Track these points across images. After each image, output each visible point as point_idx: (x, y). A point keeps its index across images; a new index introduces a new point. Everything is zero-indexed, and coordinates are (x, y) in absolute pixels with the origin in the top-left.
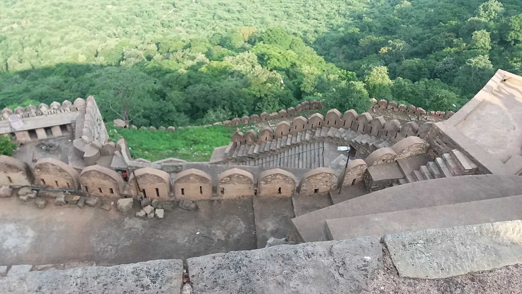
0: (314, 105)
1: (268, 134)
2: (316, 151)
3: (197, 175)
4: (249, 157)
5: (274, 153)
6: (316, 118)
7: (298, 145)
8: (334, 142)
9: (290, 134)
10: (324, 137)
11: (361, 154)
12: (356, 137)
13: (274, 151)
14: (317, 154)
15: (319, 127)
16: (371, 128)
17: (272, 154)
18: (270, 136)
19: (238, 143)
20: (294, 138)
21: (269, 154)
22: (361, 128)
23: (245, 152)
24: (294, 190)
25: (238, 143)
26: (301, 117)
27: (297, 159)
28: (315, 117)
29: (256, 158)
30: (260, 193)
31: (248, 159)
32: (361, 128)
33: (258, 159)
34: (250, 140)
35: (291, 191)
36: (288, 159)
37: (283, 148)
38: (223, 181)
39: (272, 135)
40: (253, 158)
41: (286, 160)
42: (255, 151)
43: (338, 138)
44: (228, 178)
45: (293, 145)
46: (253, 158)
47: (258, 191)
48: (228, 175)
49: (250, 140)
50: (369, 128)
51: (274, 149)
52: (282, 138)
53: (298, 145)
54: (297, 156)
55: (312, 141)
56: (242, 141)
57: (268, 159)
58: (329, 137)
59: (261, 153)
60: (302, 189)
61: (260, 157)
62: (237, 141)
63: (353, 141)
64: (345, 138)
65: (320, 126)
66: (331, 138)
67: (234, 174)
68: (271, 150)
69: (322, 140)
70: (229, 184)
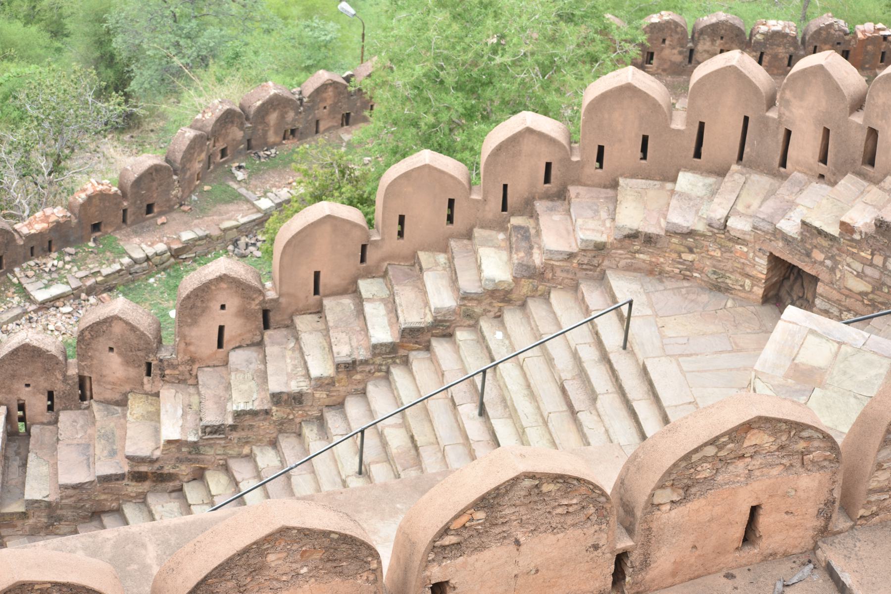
0: (273, 118)
1: (233, 303)
2: (581, 338)
3: (306, 533)
4: (139, 477)
5: (298, 414)
6: (527, 145)
7: (442, 327)
8: (666, 262)
9: (368, 274)
10: (600, 248)
11: (849, 293)
12: (792, 205)
13: (297, 399)
14: (589, 354)
15: (548, 197)
16: (873, 133)
17: (283, 426)
18: (244, 313)
19: (37, 405)
20: (405, 295)
21: (265, 427)
22: (805, 148)
23: (100, 449)
24: (830, 503)
25: (37, 405)
26: (426, 157)
27: (468, 410)
28: (514, 140)
29: (184, 470)
30: (646, 563)
31: (134, 488)
32: (805, 148)
33: (199, 476)
34: (114, 367)
35: (813, 511)
36: (405, 425)
37: (349, 367)
38: (449, 540)
39: (255, 306)
40: (161, 478)
41: (397, 439)
42: (171, 430)
43: (691, 233)
44: (480, 515)
45: (416, 338)
46: (161, 478)
47: (635, 557)
48: (474, 495)
49: (114, 367)
50: (860, 139)
51: (294, 386)
52: (319, 311)
53: (442, 327)
54: (460, 393)
55: (526, 287)
56: (59, 387)
57: (267, 459)
58: (634, 236)
59: (216, 430)
60: (863, 489)
61: (210, 454)
62: (25, 394)
63: (790, 226)
64: (738, 225)
65: (552, 187)
66: (649, 240)
67: (516, 480)
68: (277, 398)
69: (593, 262)
70: (482, 547)
